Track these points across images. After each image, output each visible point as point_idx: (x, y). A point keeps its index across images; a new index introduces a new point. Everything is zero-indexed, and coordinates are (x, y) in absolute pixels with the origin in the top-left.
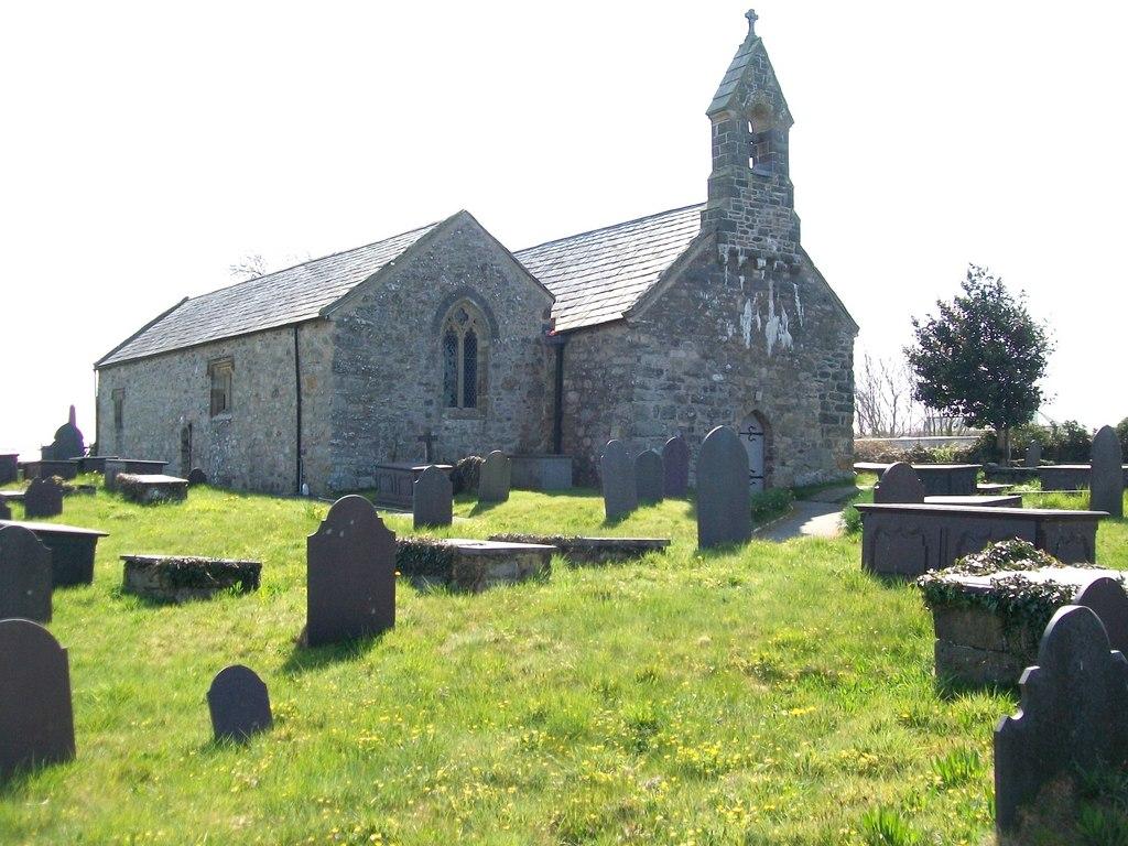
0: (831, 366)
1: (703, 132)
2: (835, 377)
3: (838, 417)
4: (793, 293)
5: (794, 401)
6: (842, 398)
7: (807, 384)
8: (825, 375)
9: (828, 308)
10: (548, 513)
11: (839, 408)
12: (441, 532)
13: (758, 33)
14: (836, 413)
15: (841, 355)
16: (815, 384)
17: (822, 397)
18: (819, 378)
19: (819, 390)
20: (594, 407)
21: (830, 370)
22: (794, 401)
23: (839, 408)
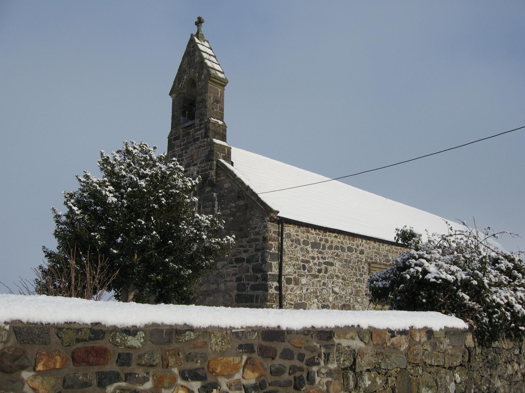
0: (245, 251)
1: (168, 103)
2: (248, 261)
3: (253, 296)
4: (213, 200)
5: (214, 286)
6: (257, 278)
7: (224, 271)
8: (240, 260)
9: (242, 203)
10: (409, 386)
11: (254, 288)
12: (266, 389)
13: (196, 27)
14: (251, 293)
15: (256, 240)
16: (230, 270)
17: (239, 280)
18: (234, 264)
19: (234, 275)
20: (190, 280)
21: (245, 256)
22: (214, 286)
23: (254, 288)
